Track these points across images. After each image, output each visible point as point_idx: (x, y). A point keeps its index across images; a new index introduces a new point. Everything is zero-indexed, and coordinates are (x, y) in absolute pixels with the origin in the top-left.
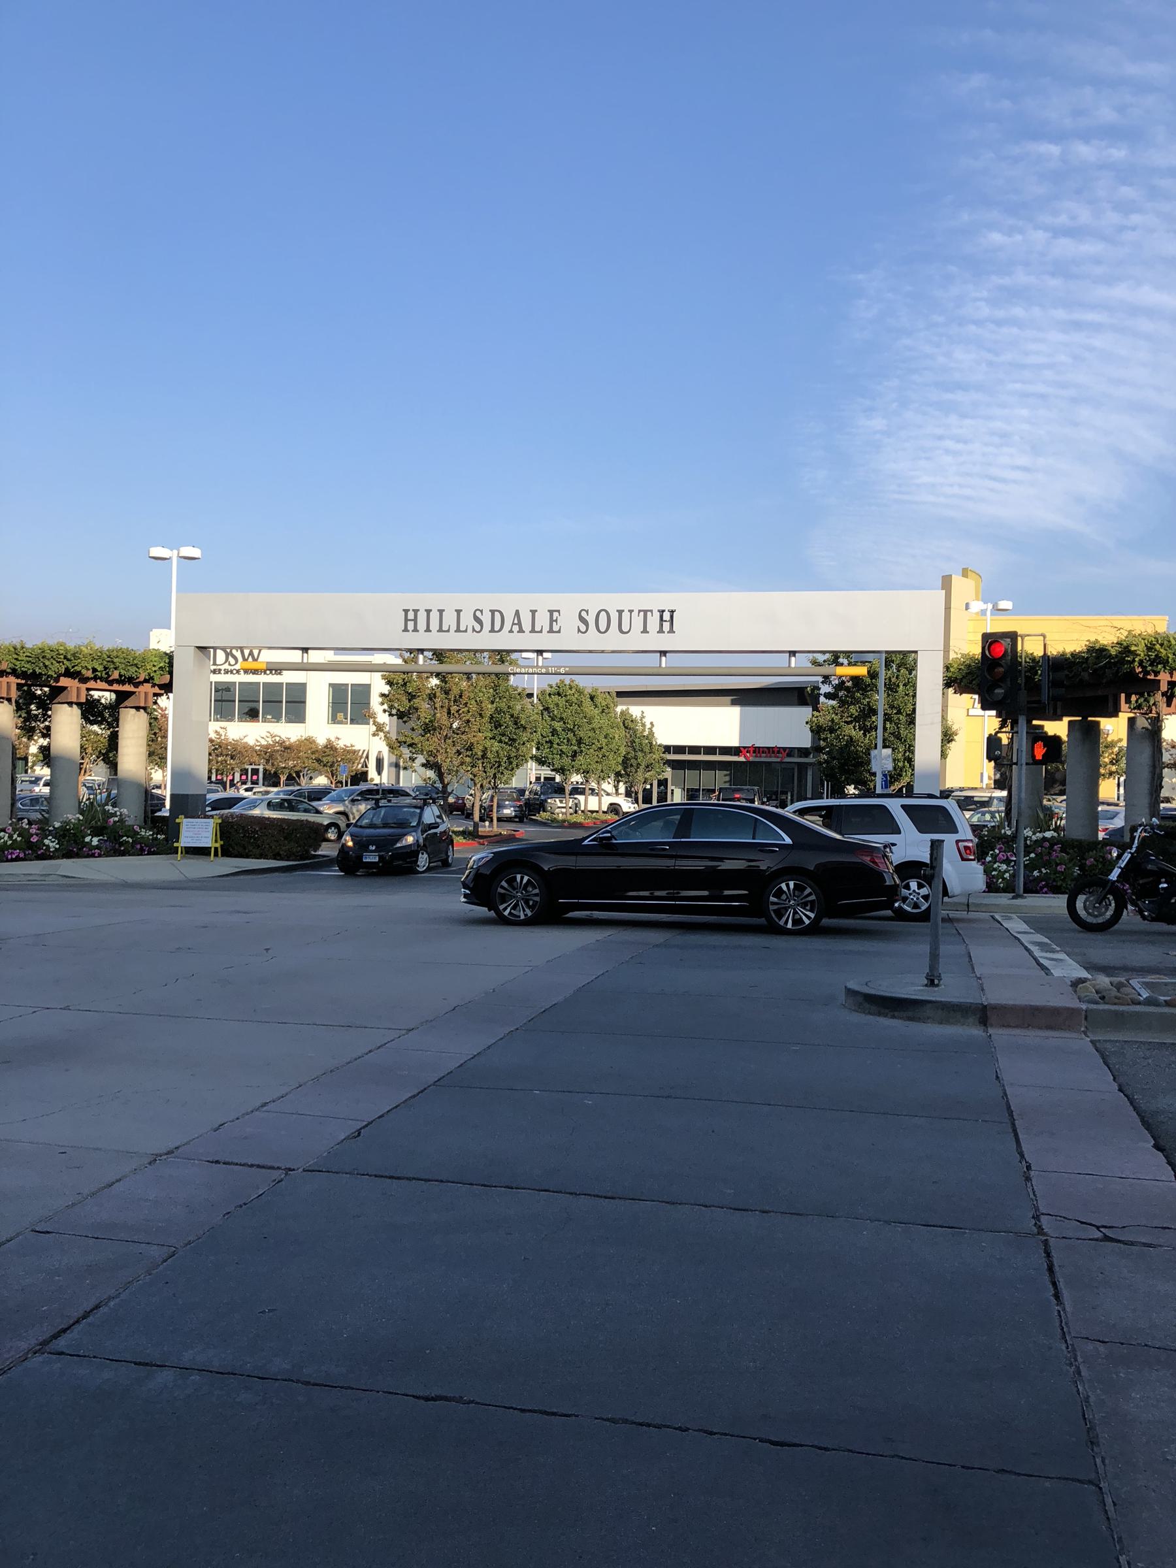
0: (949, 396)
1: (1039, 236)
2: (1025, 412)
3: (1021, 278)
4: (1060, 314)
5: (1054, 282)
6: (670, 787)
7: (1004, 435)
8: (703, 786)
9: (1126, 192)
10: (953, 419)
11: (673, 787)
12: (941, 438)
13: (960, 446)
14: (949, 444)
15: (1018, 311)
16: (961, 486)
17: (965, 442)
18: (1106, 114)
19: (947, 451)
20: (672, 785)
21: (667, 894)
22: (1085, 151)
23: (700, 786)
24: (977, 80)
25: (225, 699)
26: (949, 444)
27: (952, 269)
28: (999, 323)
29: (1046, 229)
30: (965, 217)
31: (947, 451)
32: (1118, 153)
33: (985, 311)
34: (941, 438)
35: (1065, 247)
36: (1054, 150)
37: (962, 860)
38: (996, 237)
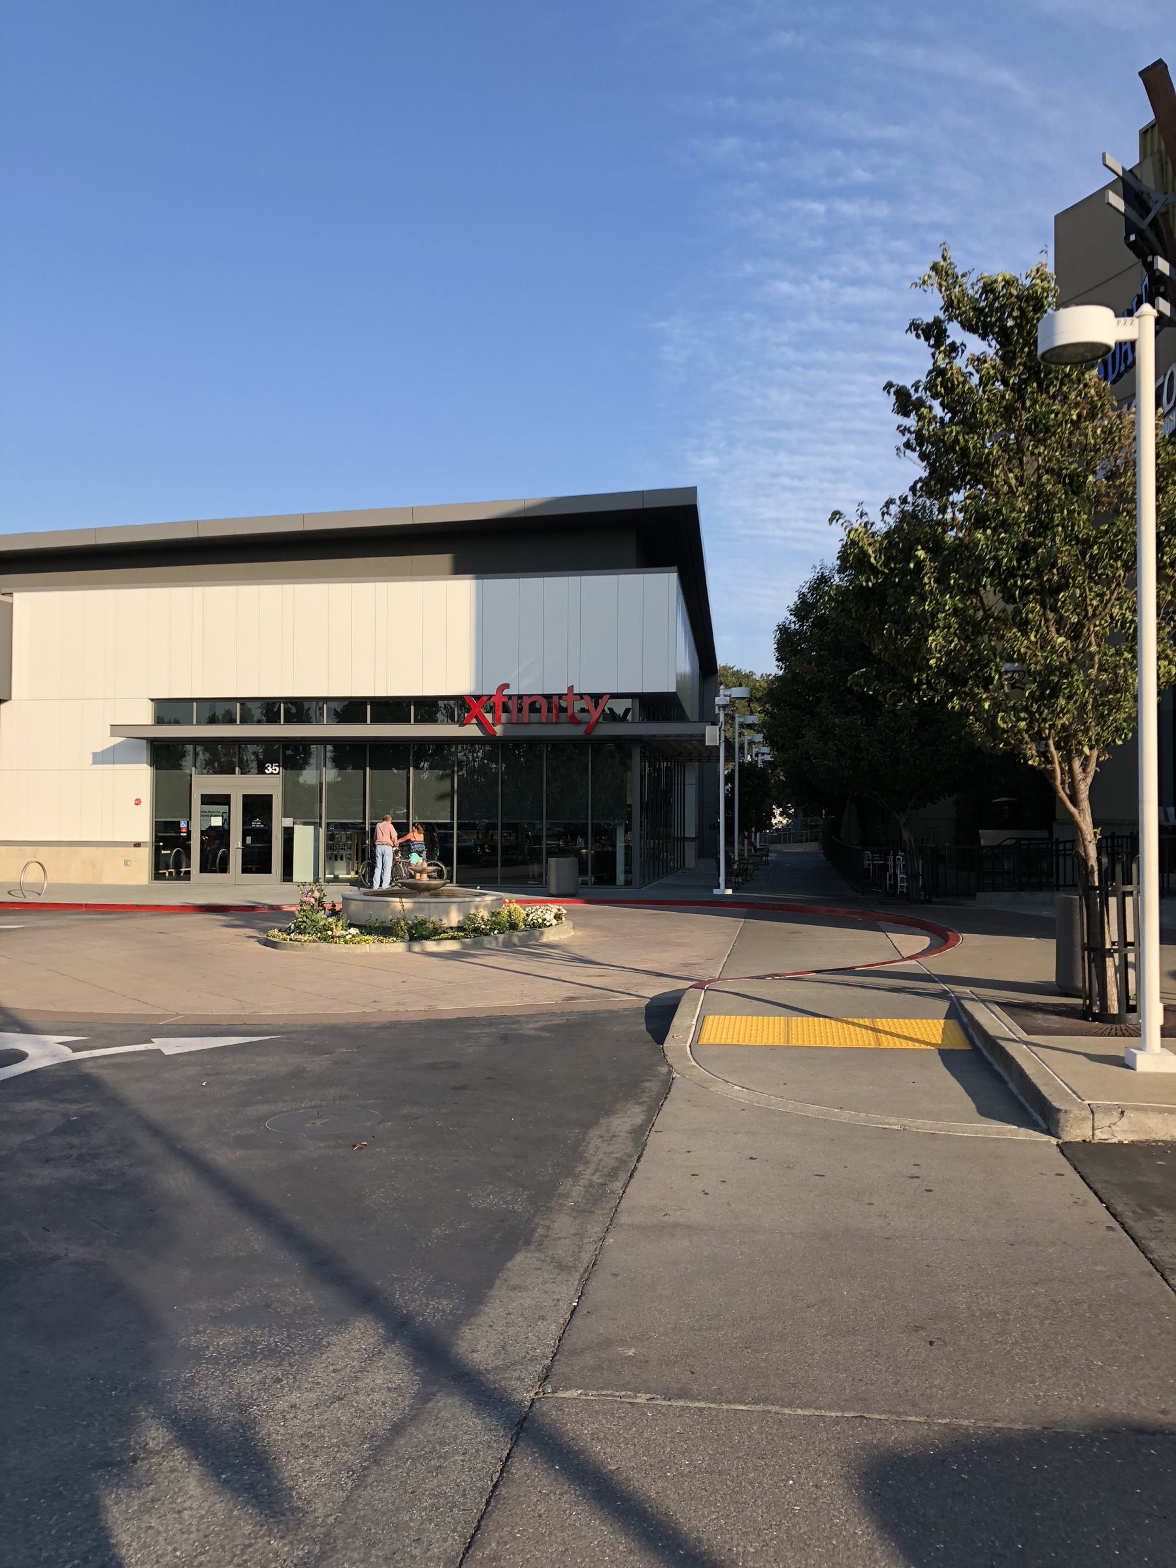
0: (774, 434)
1: (826, 285)
2: (852, 448)
3: (815, 322)
4: (863, 357)
5: (851, 328)
6: (279, 822)
7: (835, 471)
8: (327, 817)
9: (896, 245)
10: (782, 456)
11: (288, 822)
12: (775, 475)
13: (795, 483)
14: (785, 480)
15: (821, 355)
16: (806, 520)
17: (801, 478)
18: (860, 175)
19: (786, 488)
20: (285, 815)
21: (1092, 866)
22: (849, 209)
23: (364, 818)
24: (730, 143)
25: (686, 846)
26: (785, 480)
27: (748, 316)
28: (807, 366)
29: (832, 279)
30: (749, 268)
31: (786, 488)
32: (882, 211)
33: (790, 354)
34: (775, 475)
35: (852, 296)
36: (819, 208)
37: (73, 1052)
38: (785, 287)
